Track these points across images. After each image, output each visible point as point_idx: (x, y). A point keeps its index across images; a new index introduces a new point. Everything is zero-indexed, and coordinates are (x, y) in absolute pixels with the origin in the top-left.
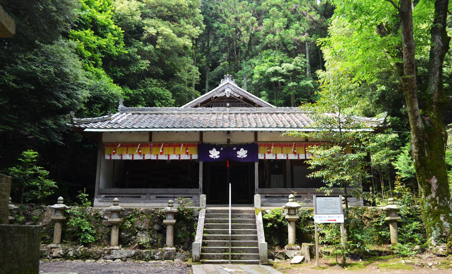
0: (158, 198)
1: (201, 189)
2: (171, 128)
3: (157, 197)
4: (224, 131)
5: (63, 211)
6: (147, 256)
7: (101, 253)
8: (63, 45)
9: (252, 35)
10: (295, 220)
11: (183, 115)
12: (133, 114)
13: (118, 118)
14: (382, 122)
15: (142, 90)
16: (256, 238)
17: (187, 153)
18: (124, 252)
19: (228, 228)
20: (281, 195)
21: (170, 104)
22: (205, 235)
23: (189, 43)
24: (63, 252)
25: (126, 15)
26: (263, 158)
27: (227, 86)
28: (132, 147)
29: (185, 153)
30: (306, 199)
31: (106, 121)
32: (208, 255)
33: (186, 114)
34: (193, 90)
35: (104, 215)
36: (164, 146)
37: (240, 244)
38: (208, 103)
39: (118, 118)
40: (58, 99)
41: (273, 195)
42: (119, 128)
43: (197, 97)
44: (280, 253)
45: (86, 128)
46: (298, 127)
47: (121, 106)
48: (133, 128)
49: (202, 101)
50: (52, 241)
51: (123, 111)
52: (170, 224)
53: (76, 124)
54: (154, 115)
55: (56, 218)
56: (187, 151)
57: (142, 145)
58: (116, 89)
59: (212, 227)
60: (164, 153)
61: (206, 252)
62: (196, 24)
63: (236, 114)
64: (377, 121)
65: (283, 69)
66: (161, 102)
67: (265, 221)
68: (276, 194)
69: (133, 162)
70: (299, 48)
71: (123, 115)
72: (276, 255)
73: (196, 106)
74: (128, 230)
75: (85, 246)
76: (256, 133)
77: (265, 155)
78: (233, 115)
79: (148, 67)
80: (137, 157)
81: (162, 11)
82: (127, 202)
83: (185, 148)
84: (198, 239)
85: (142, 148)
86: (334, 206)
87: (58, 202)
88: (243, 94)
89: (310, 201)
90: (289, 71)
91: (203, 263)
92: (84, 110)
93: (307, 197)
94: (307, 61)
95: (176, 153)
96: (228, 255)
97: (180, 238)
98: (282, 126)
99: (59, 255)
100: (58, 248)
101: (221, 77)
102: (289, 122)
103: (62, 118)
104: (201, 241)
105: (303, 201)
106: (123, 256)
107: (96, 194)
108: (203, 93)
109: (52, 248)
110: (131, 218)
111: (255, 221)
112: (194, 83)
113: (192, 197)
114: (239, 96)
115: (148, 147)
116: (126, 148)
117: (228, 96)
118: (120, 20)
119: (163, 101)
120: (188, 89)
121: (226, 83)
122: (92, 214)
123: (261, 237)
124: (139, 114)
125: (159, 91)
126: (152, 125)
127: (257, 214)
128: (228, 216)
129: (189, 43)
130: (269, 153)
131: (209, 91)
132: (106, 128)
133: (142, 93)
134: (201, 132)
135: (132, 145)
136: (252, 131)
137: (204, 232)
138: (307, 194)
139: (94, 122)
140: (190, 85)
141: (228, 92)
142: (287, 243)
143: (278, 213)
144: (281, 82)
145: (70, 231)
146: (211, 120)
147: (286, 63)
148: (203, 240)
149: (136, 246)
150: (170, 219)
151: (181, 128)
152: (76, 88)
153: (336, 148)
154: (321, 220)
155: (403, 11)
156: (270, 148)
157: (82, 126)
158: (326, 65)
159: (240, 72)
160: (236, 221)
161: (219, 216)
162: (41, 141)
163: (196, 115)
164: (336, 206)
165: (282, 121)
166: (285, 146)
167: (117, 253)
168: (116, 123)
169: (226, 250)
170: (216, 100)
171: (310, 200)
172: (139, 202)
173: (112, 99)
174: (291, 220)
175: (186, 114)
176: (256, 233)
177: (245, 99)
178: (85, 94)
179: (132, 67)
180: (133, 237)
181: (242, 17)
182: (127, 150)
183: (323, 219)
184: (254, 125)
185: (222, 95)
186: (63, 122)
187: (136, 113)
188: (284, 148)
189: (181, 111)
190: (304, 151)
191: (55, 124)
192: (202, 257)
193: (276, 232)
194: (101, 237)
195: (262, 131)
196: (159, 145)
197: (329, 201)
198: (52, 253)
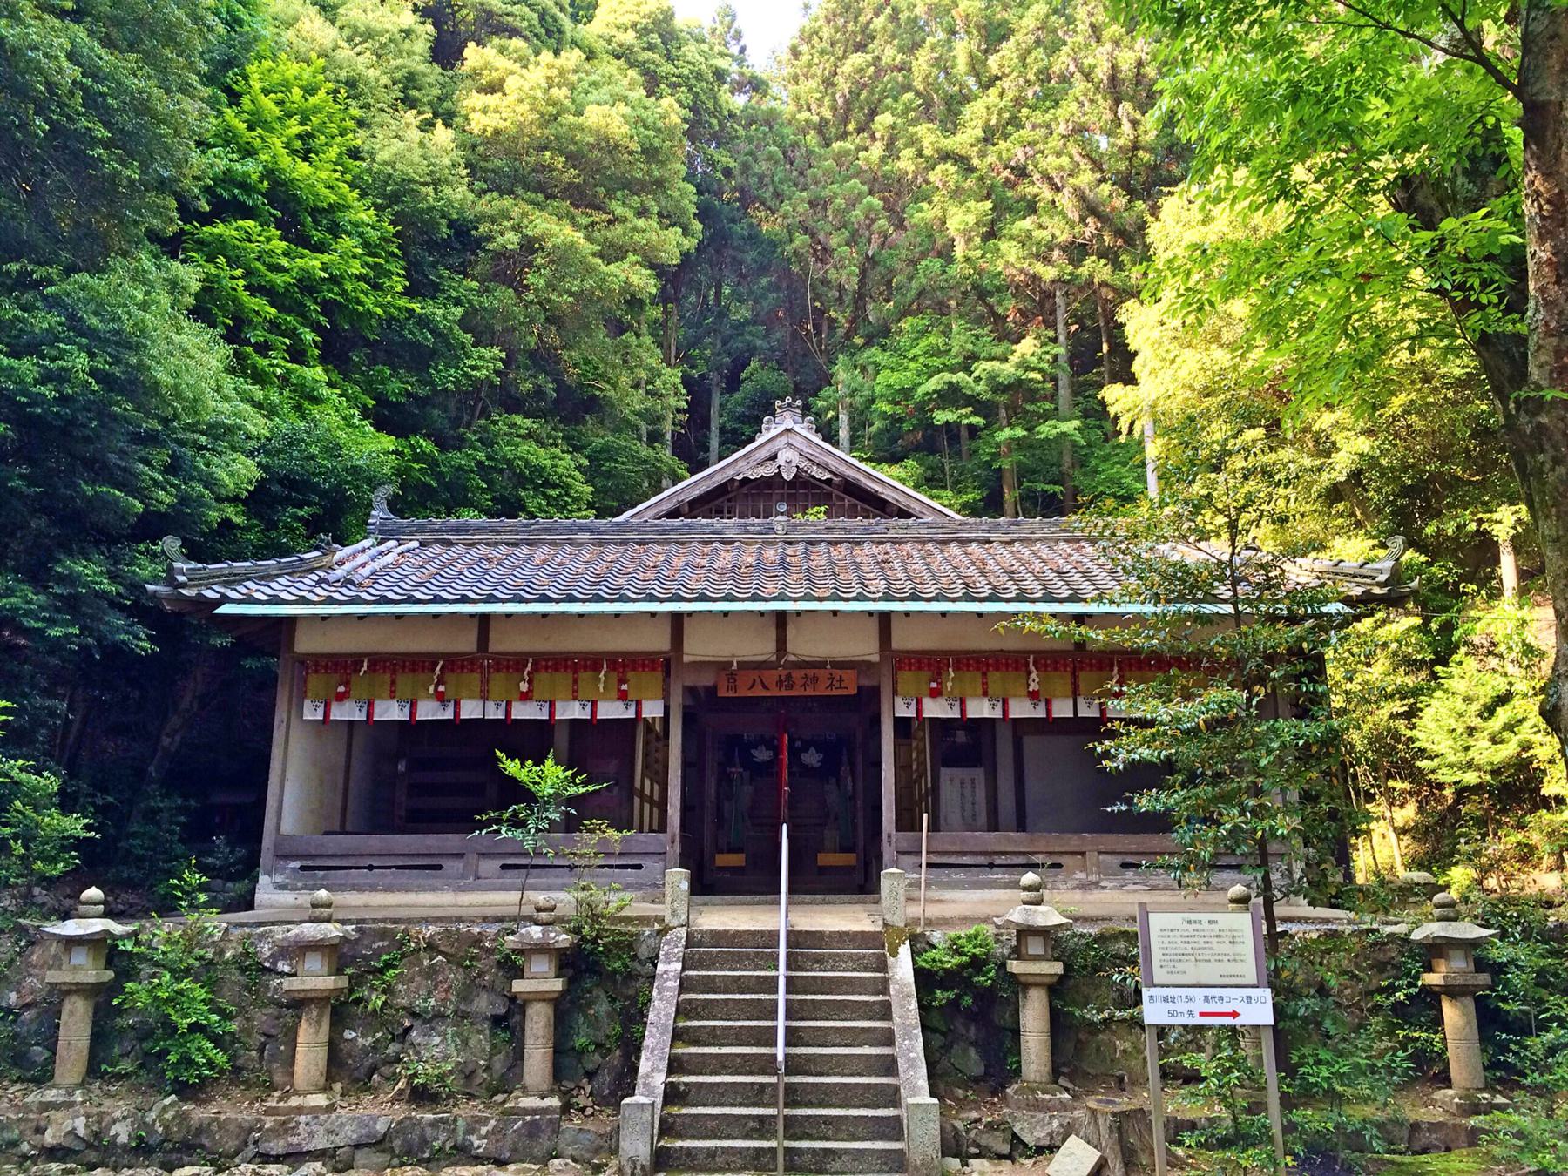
1: (673, 837)
4: (762, 614)
5: (101, 945)
6: (440, 1140)
7: (251, 1130)
8: (138, 277)
9: (871, 262)
11: (612, 547)
12: (423, 544)
13: (361, 559)
14: (1382, 578)
15: (481, 456)
16: (889, 1066)
17: (623, 696)
18: (342, 1125)
20: (981, 860)
21: (576, 500)
23: (645, 282)
24: (87, 1126)
25: (411, 181)
26: (911, 713)
27: (784, 439)
28: (413, 671)
29: (614, 694)
30: (1080, 875)
31: (311, 571)
32: (689, 1152)
33: (624, 542)
34: (666, 454)
35: (274, 958)
36: (535, 668)
38: (716, 502)
39: (361, 559)
40: (128, 483)
41: (952, 860)
43: (676, 479)
45: (224, 599)
46: (1049, 598)
47: (379, 514)
48: (411, 600)
51: (385, 533)
52: (540, 997)
53: (184, 585)
55: (67, 977)
56: (624, 687)
58: (374, 448)
59: (709, 1010)
60: (536, 696)
62: (669, 219)
63: (811, 543)
64: (1363, 571)
65: (978, 379)
66: (545, 496)
67: (925, 979)
68: (964, 854)
69: (410, 729)
70: (1039, 303)
71: (382, 548)
74: (377, 1019)
76: (885, 618)
77: (919, 702)
80: (429, 711)
81: (551, 168)
82: (388, 889)
83: (614, 676)
85: (449, 677)
86: (1226, 948)
88: (843, 469)
90: (998, 387)
93: (1084, 869)
94: (1061, 350)
96: (773, 1150)
97: (581, 1053)
98: (987, 591)
100: (71, 1105)
101: (763, 408)
102: (1011, 573)
103: (141, 553)
104: (659, 1080)
105: (1070, 884)
106: (338, 1141)
107: (266, 857)
108: (697, 466)
109: (46, 1106)
110: (389, 965)
112: (668, 428)
113: (639, 867)
114: (828, 476)
115: (472, 671)
117: (788, 476)
118: (395, 198)
119: (554, 493)
120: (644, 451)
121: (781, 428)
122: (228, 955)
124: (449, 543)
125: (540, 456)
126: (484, 590)
127: (895, 954)
128: (775, 957)
129: (645, 282)
130: (935, 694)
131: (721, 459)
132: (303, 601)
133: (480, 464)
135: (414, 663)
136: (871, 614)
137: (678, 1036)
138: (1083, 854)
139: (262, 578)
141: (788, 462)
142: (1018, 1072)
143: (976, 951)
144: (970, 426)
145: (132, 1027)
146: (711, 570)
148: (670, 1072)
149: (401, 1092)
151: (598, 599)
152: (203, 439)
153: (1218, 696)
154: (1171, 1013)
156: (939, 674)
157: (209, 594)
158: (1136, 367)
159: (827, 391)
161: (737, 961)
162: (56, 646)
163: (659, 548)
164: (1238, 948)
165: (983, 574)
166: (997, 669)
167: (315, 1128)
168: (348, 581)
170: (744, 490)
171: (1094, 878)
172: (434, 889)
173: (357, 488)
174: (1031, 980)
175: (624, 542)
176: (888, 1038)
178: (240, 471)
179: (438, 372)
180: (392, 1049)
181: (835, 195)
182: (393, 683)
183: (1181, 1007)
184: (878, 587)
185: (768, 471)
186: (144, 570)
187: (437, 541)
188: (994, 676)
190: (1069, 688)
191: (113, 577)
194: (261, 1050)
195: (907, 614)
196: (518, 662)
197: (1206, 926)
198: (40, 1131)
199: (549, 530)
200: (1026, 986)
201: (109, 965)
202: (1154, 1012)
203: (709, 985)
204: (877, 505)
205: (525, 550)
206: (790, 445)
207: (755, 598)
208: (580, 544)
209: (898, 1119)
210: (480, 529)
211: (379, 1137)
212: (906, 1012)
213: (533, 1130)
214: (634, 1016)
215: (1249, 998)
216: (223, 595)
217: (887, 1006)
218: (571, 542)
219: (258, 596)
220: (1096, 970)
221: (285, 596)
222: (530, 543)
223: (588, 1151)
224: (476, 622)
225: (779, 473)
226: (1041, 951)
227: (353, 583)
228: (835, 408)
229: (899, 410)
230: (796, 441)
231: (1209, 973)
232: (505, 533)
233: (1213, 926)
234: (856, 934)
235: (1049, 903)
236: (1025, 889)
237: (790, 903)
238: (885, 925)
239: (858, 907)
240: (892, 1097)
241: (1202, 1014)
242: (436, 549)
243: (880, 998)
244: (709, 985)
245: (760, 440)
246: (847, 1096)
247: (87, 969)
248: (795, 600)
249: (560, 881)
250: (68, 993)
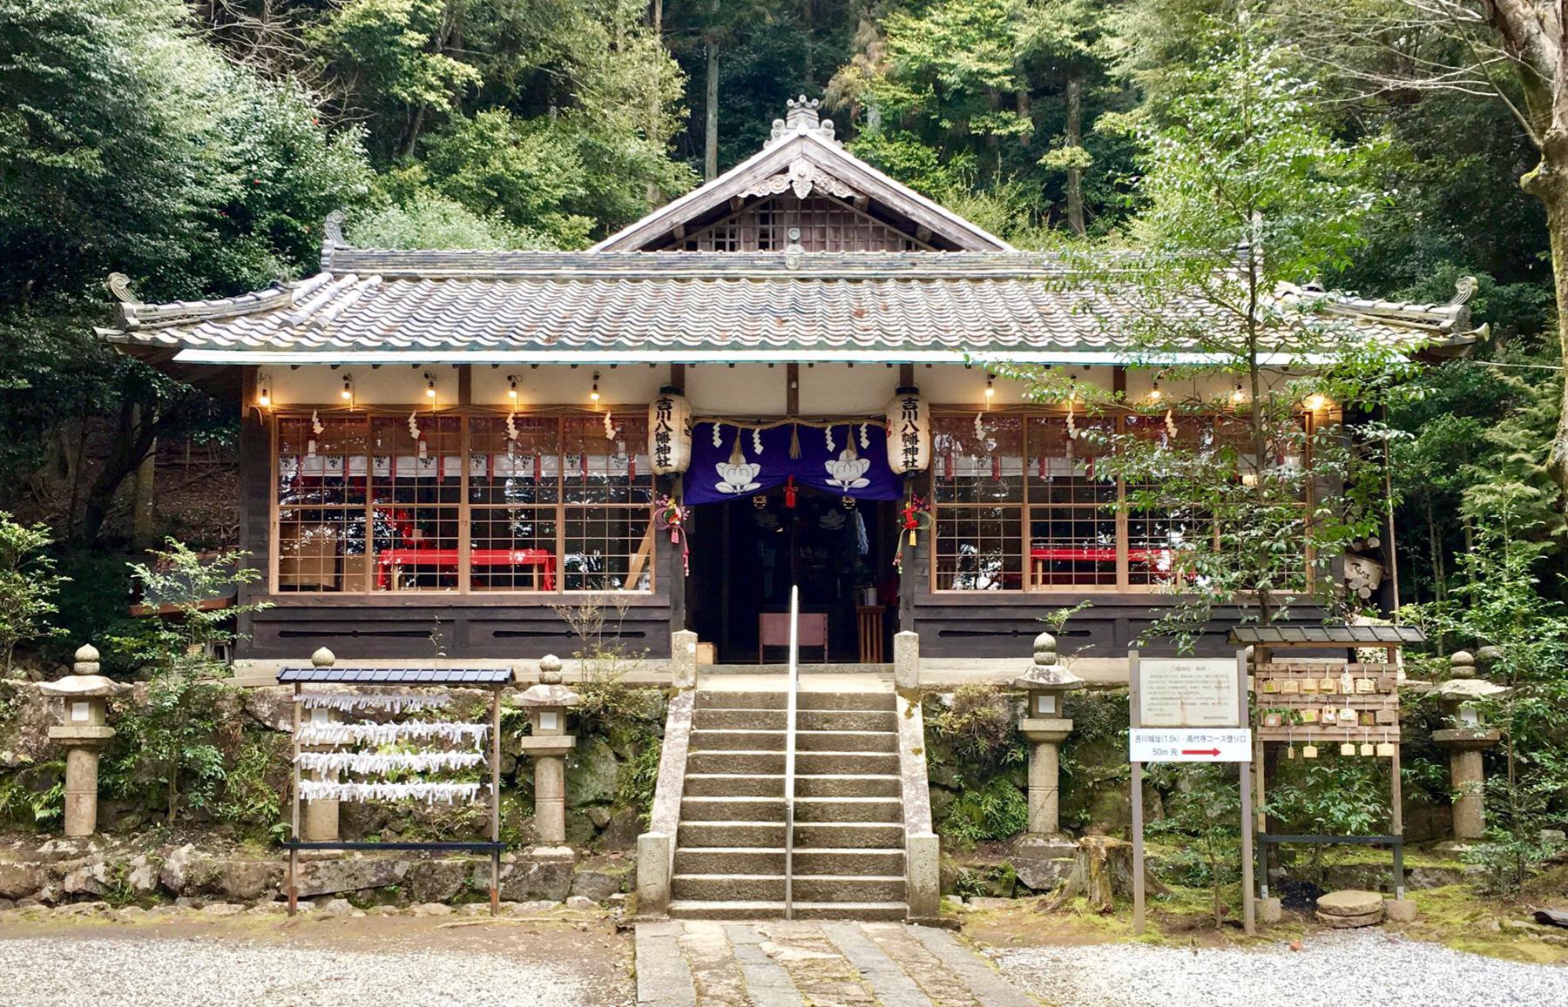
0: (505, 640)
3: (497, 634)
10: (1057, 737)
13: (323, 297)
19: (781, 768)
20: (1009, 628)
27: (796, 148)
31: (270, 311)
33: (615, 279)
37: (833, 838)
39: (323, 297)
42: (326, 347)
48: (386, 347)
49: (692, 214)
53: (136, 329)
54: (477, 285)
63: (826, 280)
64: (1428, 317)
73: (666, 241)
84: (664, 810)
87: (78, 666)
91: (673, 914)
114: (850, 193)
117: (801, 193)
121: (794, 135)
124: (417, 279)
126: (465, 336)
131: (719, 174)
132: (269, 347)
139: (216, 320)
150: (550, 733)
151: (593, 347)
154: (1156, 752)
157: (164, 338)
160: (818, 743)
164: (1224, 692)
169: (777, 863)
174: (1039, 736)
175: (615, 279)
176: (895, 790)
177: (877, 208)
185: (778, 186)
189: (593, 266)
192: (677, 891)
200: (1036, 743)
201: (110, 723)
203: (719, 742)
205: (502, 286)
206: (804, 155)
207: (763, 346)
209: (901, 856)
215: (1230, 737)
217: (896, 761)
219: (218, 340)
220: (1099, 724)
222: (508, 279)
224: (456, 371)
225: (792, 189)
226: (1053, 711)
227: (319, 327)
230: (811, 150)
233: (1202, 672)
234: (867, 696)
240: (897, 839)
241: (1185, 752)
244: (719, 742)
245: (769, 147)
247: (83, 724)
250: (73, 747)
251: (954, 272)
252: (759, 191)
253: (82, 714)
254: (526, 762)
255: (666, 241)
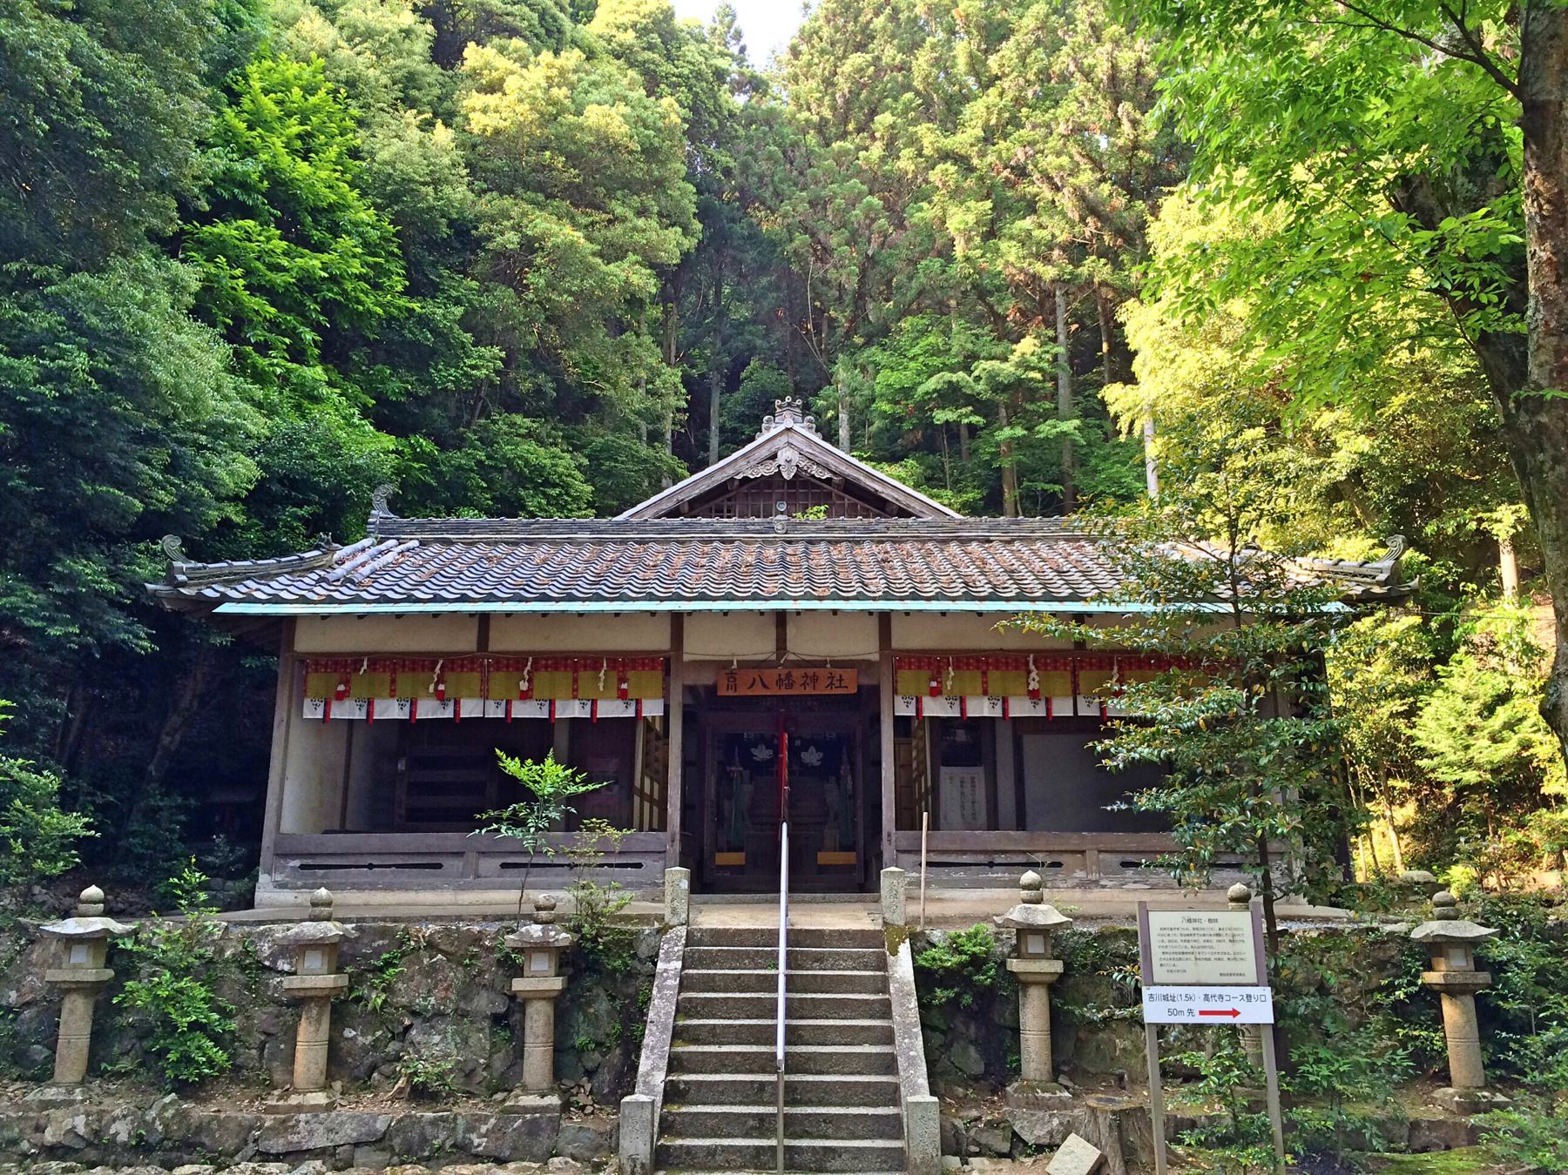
2: (557, 600)
3: (504, 866)
4: (761, 613)
8: (138, 277)
12: (423, 543)
13: (361, 558)
14: (1382, 577)
15: (481, 455)
16: (889, 1064)
17: (623, 695)
18: (342, 1123)
20: (981, 858)
21: (576, 499)
22: (682, 1049)
23: (645, 281)
24: (87, 1124)
25: (411, 180)
27: (784, 439)
28: (413, 670)
29: (614, 692)
30: (1080, 874)
31: (311, 570)
33: (624, 542)
34: (666, 453)
35: (274, 957)
38: (716, 501)
39: (361, 558)
40: (127, 482)
42: (356, 600)
43: (676, 479)
44: (989, 1124)
46: (1049, 597)
47: (379, 514)
50: (52, 1075)
51: (385, 533)
53: (184, 584)
56: (624, 686)
57: (453, 662)
58: (375, 447)
59: (709, 1008)
60: (536, 694)
61: (680, 1135)
62: (669, 218)
64: (1363, 570)
65: (978, 379)
66: (545, 495)
68: (964, 852)
69: (410, 728)
70: (1039, 303)
71: (382, 547)
72: (972, 1133)
73: (674, 513)
74: (377, 1017)
75: (184, 1097)
76: (885, 617)
77: (919, 701)
78: (800, 547)
79: (498, 372)
80: (429, 710)
82: (388, 888)
83: (614, 675)
85: (449, 676)
86: (1225, 946)
89: (1096, 882)
90: (998, 387)
92: (237, 525)
93: (1084, 868)
94: (1061, 350)
95: (581, 694)
96: (773, 1149)
98: (987, 590)
99: (69, 1141)
100: (71, 1103)
101: (763, 407)
102: (1010, 572)
104: (659, 1078)
105: (1070, 883)
107: (266, 856)
108: (697, 465)
110: (389, 964)
111: (885, 981)
112: (667, 427)
113: (639, 866)
114: (827, 475)
115: (472, 670)
116: (387, 676)
118: (395, 198)
119: (554, 492)
121: (781, 428)
122: (228, 953)
123: (912, 1062)
126: (484, 588)
127: (895, 952)
128: (775, 956)
129: (645, 281)
130: (935, 693)
131: (720, 459)
132: (303, 600)
133: (480, 463)
134: (677, 618)
135: (414, 662)
136: (870, 613)
137: (678, 1034)
138: (1082, 852)
139: (262, 577)
140: (654, 437)
141: (788, 461)
142: (1017, 1071)
143: (976, 949)
144: (970, 425)
145: (132, 1026)
146: (711, 569)
147: (987, 359)
148: (670, 1071)
149: (401, 1090)
151: (598, 598)
152: (203, 439)
154: (1171, 1012)
155: (1542, 98)
156: (939, 673)
157: (209, 593)
158: (1136, 366)
159: (827, 390)
164: (1238, 947)
165: (983, 573)
168: (347, 581)
170: (744, 489)
171: (1094, 877)
172: (434, 888)
174: (1031, 978)
175: (624, 542)
176: (888, 1037)
178: (241, 470)
180: (392, 1047)
181: (835, 195)
182: (393, 681)
183: (1182, 1005)
184: (879, 585)
185: (768, 470)
187: (437, 540)
188: (994, 675)
193: (968, 1005)
197: (1206, 924)
198: (40, 1129)
199: (549, 530)
200: (1026, 985)
202: (1154, 1010)
203: (709, 984)
204: (877, 505)
205: (525, 549)
206: (789, 444)
208: (580, 544)
210: (480, 528)
211: (379, 1135)
212: (907, 1010)
213: (532, 1129)
214: (634, 1015)
215: (1249, 996)
216: (223, 594)
217: (887, 1005)
218: (571, 542)
219: (258, 595)
220: (1096, 969)
221: (285, 595)
222: (530, 542)
223: (588, 1149)
224: (476, 621)
226: (1041, 951)
227: (353, 582)
228: (835, 408)
229: (899, 409)
231: (1210, 971)
232: (505, 532)
235: (1049, 902)
236: (1025, 887)
237: (790, 902)
238: (885, 923)
239: (858, 906)
240: (891, 1095)
241: (1202, 1013)
242: (436, 548)
243: (880, 996)
244: (709, 984)
245: (759, 440)
246: (847, 1094)
247: (87, 968)
248: (795, 599)
249: (560, 880)
250: (68, 991)
251: (924, 533)
252: (752, 474)
253: (80, 956)
254: (518, 1004)
255: (674, 513)
